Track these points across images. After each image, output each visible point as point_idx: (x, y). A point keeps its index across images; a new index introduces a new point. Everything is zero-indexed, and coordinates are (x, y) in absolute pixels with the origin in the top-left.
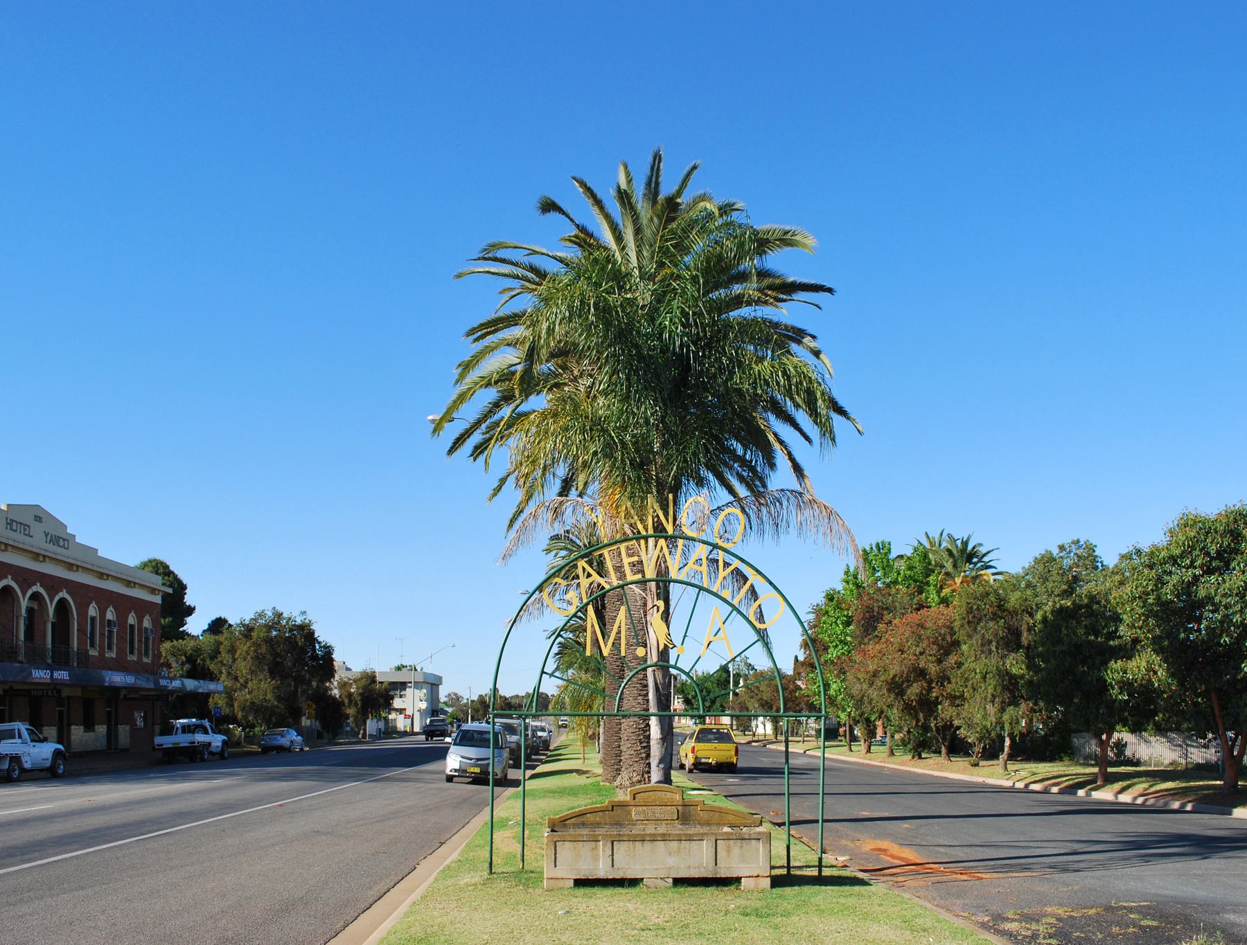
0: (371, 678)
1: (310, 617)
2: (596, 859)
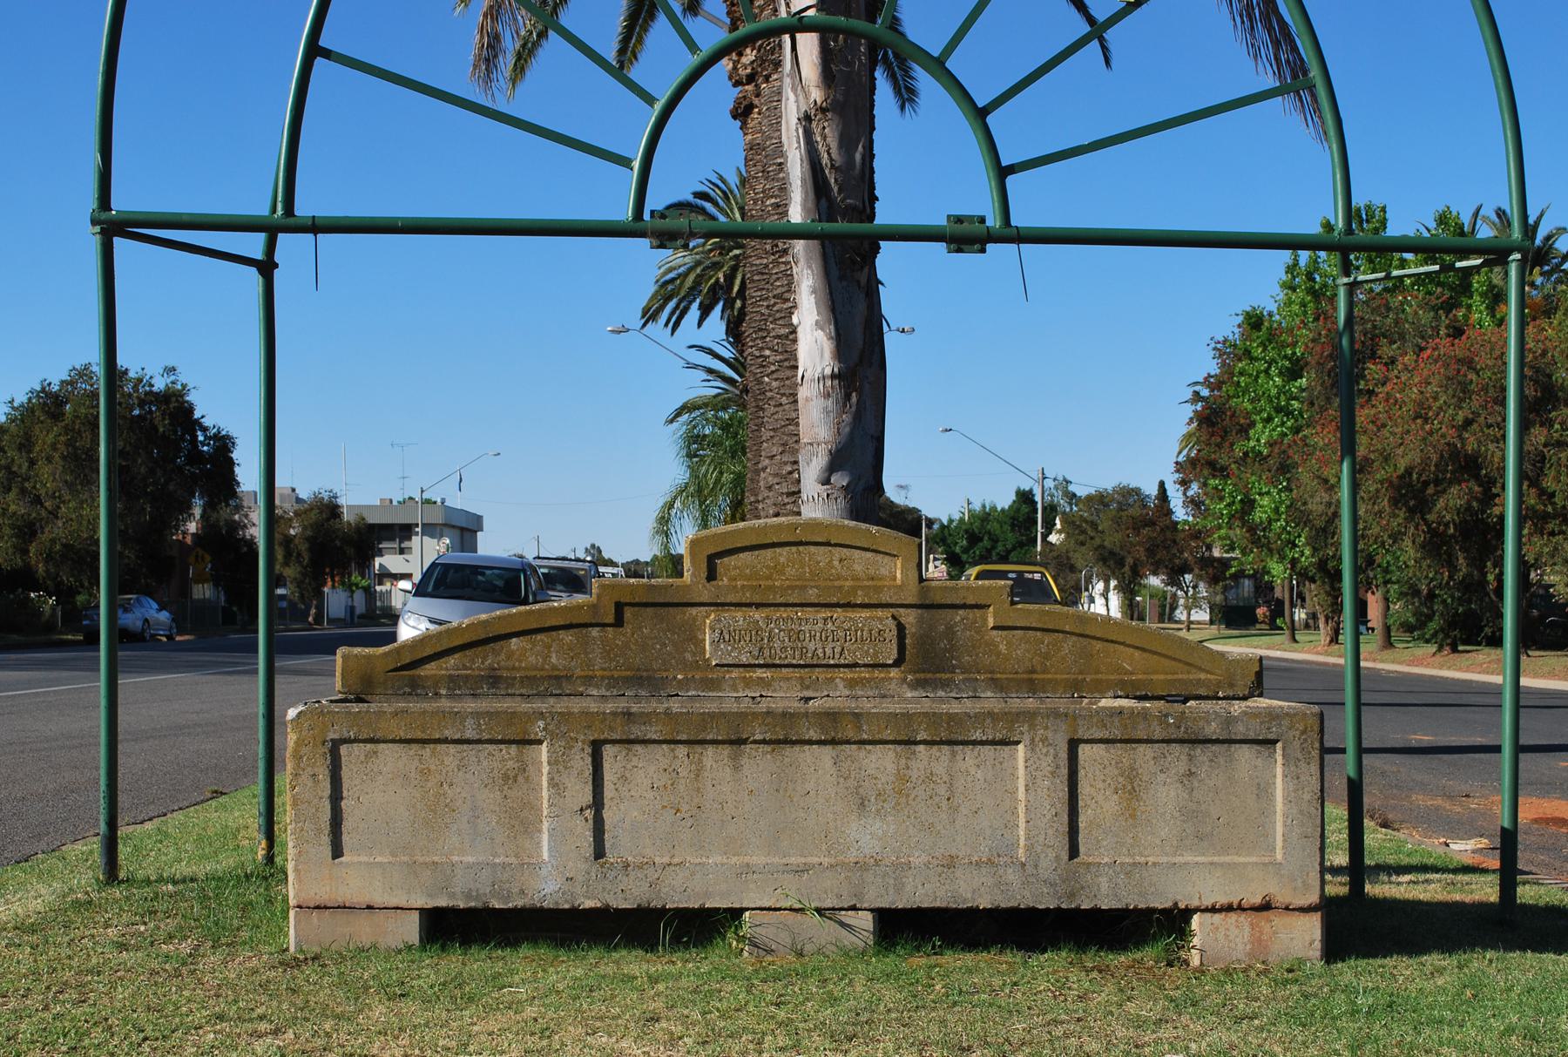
0: (328, 509)
1: (184, 377)
2: (522, 822)
